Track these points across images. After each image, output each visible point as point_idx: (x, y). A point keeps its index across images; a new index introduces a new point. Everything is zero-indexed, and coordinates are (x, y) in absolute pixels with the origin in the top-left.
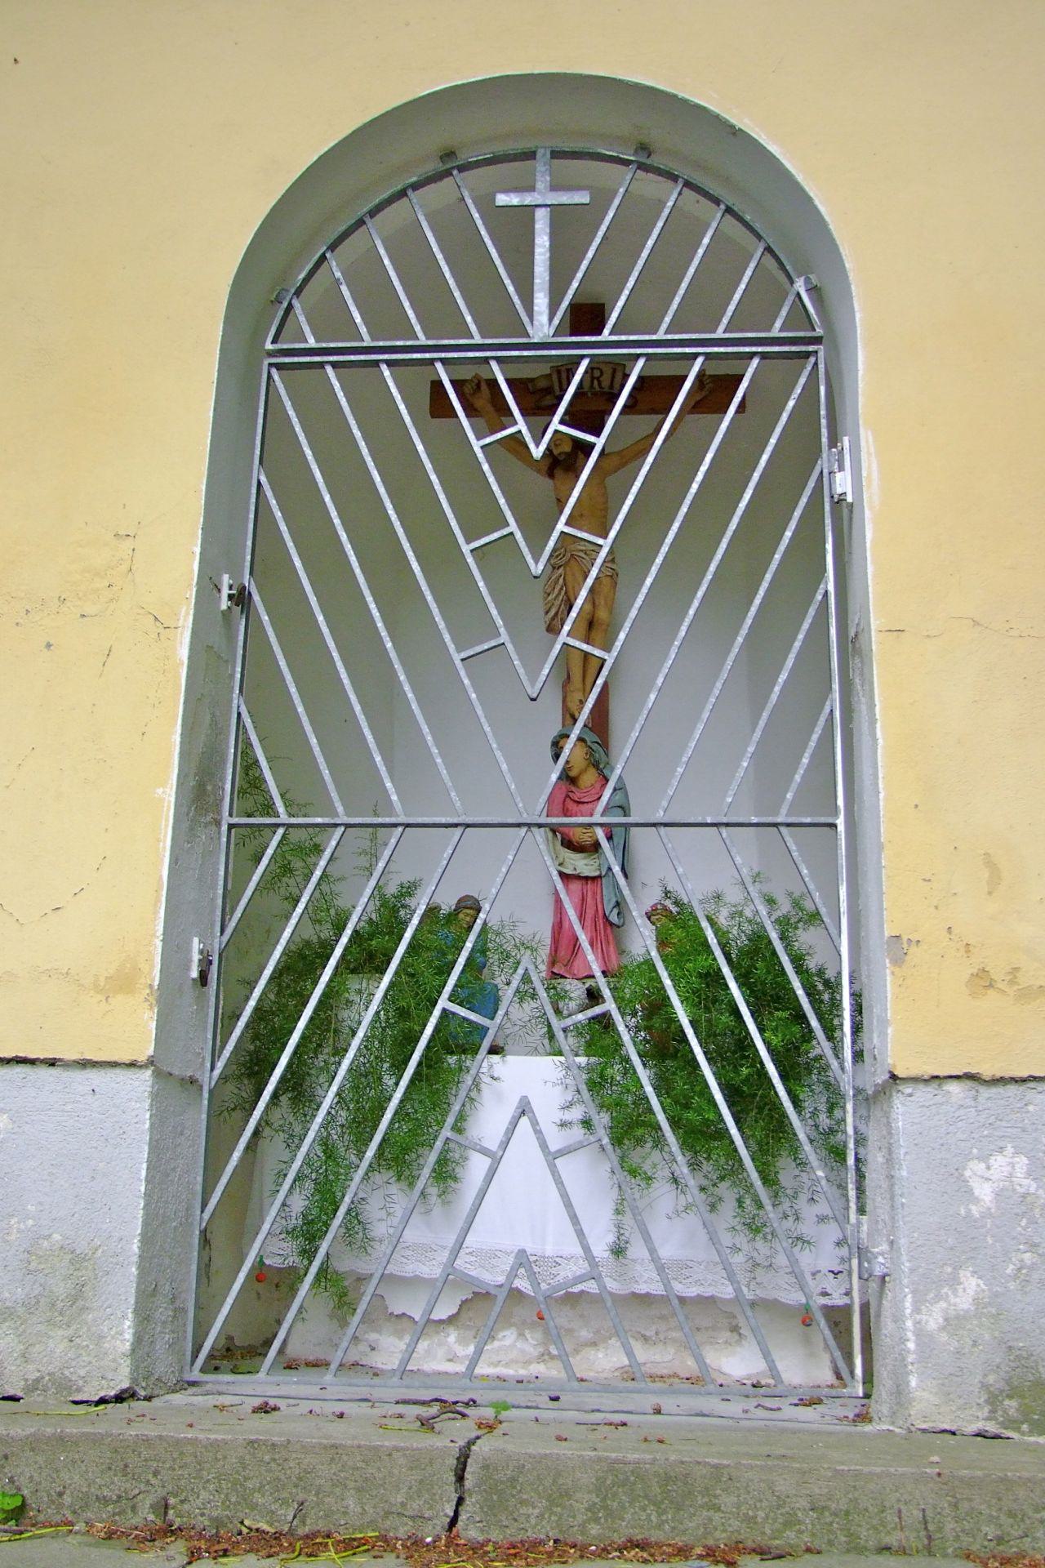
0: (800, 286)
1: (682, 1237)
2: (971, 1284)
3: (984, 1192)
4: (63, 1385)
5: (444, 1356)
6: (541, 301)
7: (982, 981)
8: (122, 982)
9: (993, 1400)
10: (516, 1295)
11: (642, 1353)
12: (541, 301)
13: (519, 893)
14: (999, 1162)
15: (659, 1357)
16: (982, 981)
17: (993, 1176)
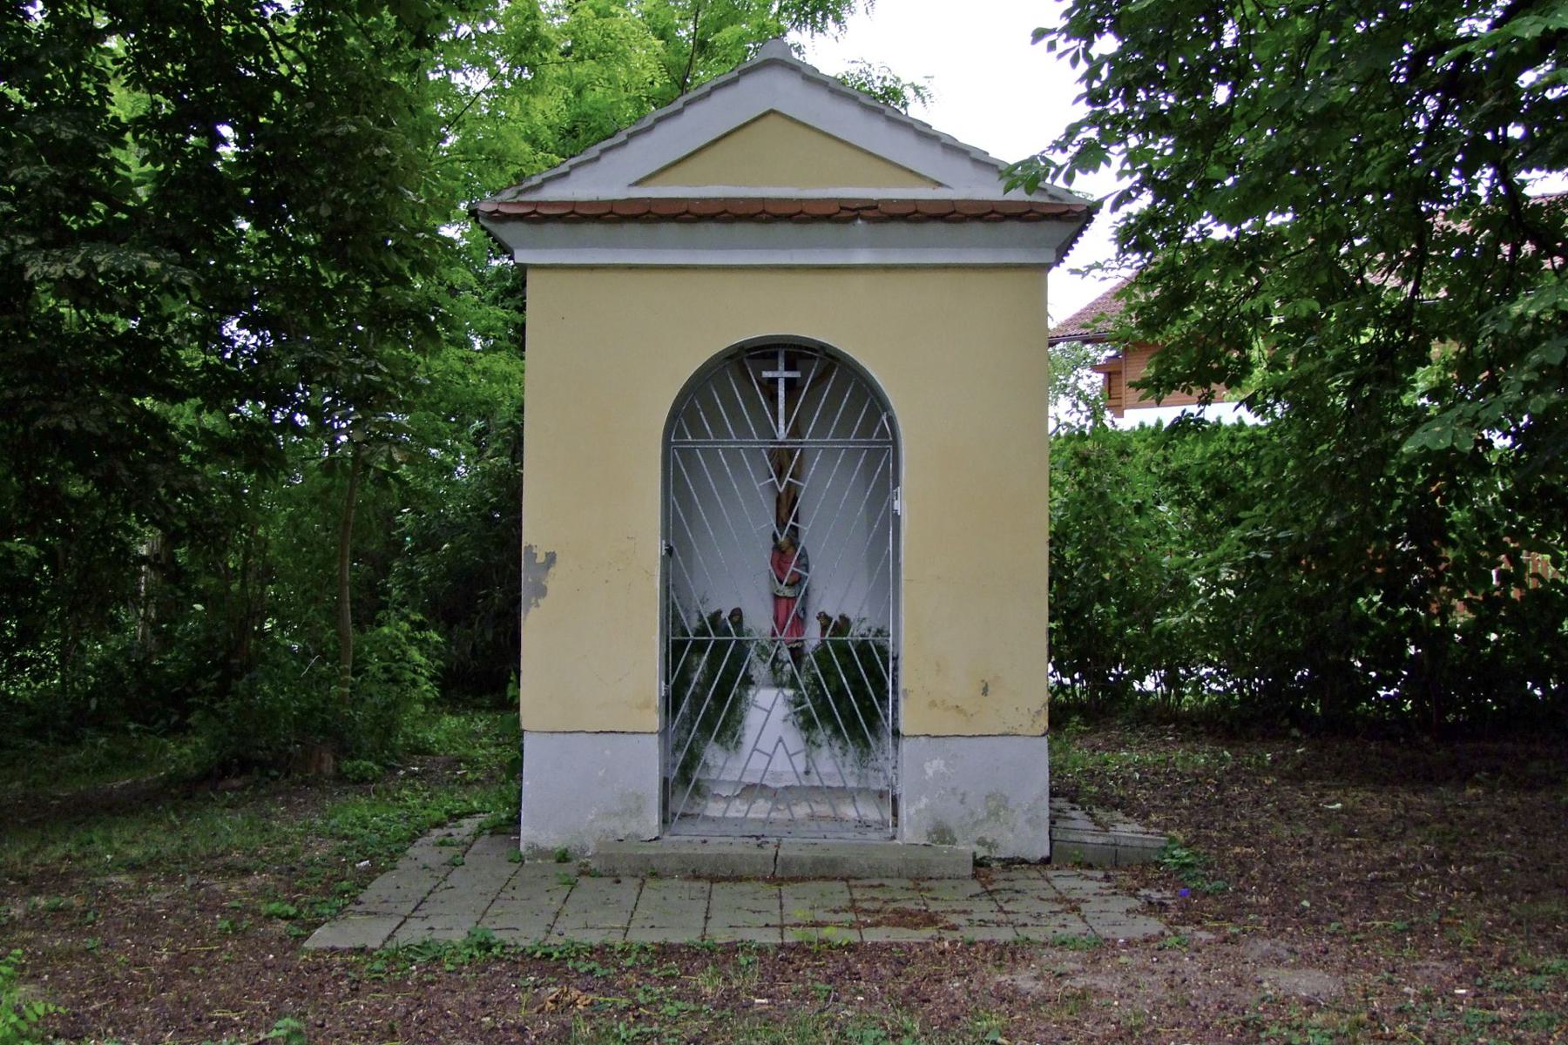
0: (884, 418)
1: (832, 763)
2: (924, 800)
3: (930, 772)
4: (638, 836)
5: (737, 809)
6: (781, 421)
7: (933, 704)
8: (646, 705)
9: (929, 835)
10: (764, 787)
11: (816, 808)
12: (781, 421)
13: (760, 621)
14: (935, 762)
15: (823, 809)
16: (933, 704)
17: (933, 767)
